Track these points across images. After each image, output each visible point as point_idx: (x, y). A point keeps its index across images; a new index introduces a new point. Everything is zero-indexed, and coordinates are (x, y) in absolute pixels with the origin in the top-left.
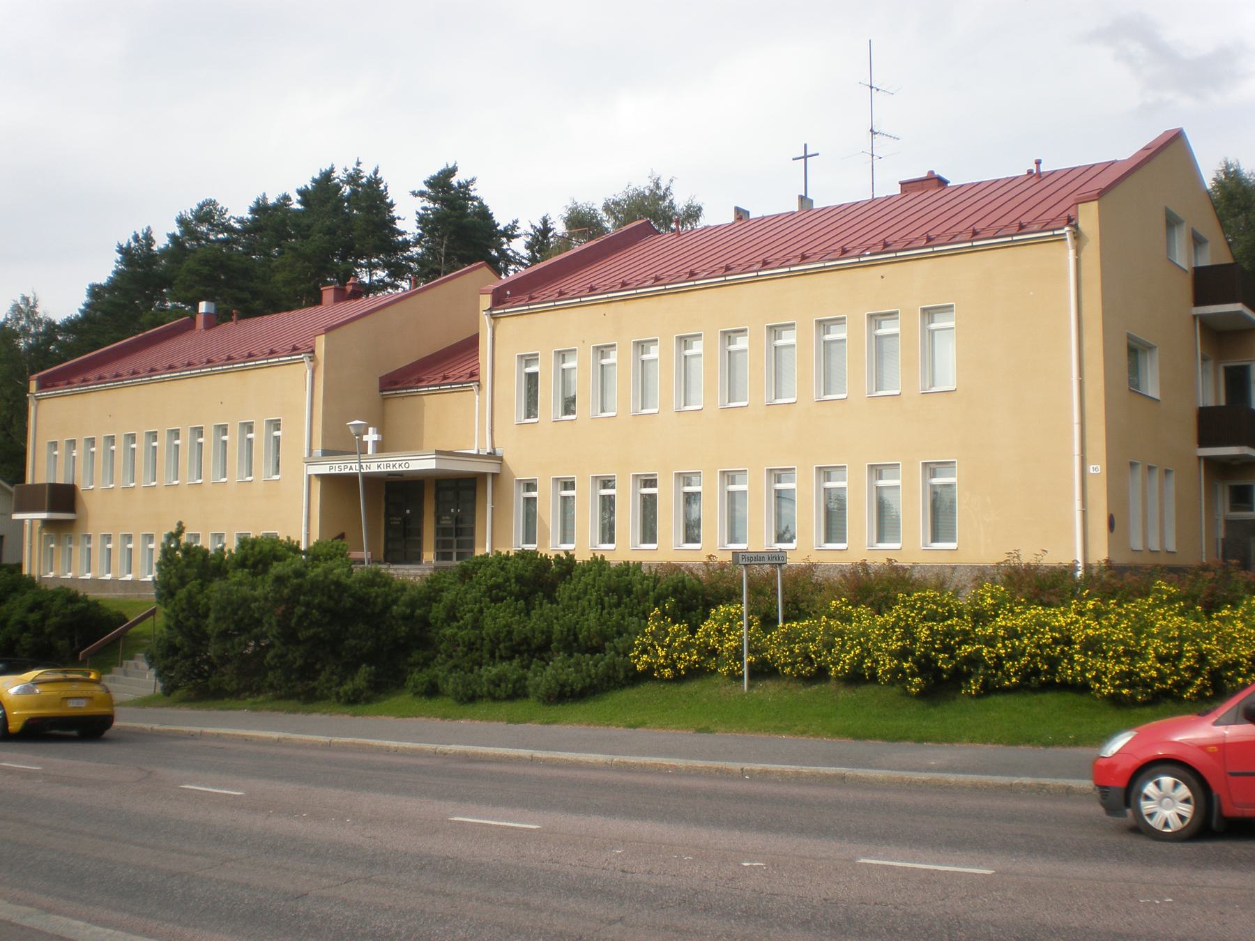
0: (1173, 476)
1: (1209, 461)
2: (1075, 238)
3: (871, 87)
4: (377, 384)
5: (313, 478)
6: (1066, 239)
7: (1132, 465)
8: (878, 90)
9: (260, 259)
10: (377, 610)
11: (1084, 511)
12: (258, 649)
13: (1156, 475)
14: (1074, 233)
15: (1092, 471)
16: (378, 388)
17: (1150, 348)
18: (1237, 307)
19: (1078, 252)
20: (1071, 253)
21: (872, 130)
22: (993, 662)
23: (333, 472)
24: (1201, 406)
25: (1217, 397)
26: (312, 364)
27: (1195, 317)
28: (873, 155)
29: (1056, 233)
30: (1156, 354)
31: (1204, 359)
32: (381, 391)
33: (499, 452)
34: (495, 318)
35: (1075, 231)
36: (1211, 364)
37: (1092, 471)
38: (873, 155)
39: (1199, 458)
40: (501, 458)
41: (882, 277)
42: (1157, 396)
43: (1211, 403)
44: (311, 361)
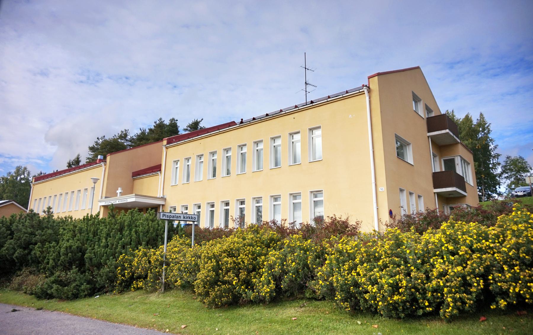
0: (422, 198)
1: (439, 195)
2: (368, 92)
3: (306, 68)
4: (131, 174)
5: (101, 207)
6: (364, 93)
7: (401, 190)
8: (308, 69)
9: (510, 292)
10: (494, 282)
11: (377, 208)
12: (197, 272)
13: (414, 197)
14: (368, 90)
15: (380, 190)
16: (132, 176)
17: (409, 144)
18: (447, 131)
19: (370, 98)
20: (367, 98)
21: (306, 83)
22: (29, 259)
23: (106, 204)
24: (434, 172)
25: (441, 168)
26: (105, 166)
27: (428, 137)
28: (306, 91)
29: (360, 91)
30: (411, 146)
31: (434, 156)
32: (132, 177)
33: (165, 197)
34: (167, 148)
35: (368, 89)
36: (437, 159)
37: (380, 190)
38: (306, 91)
39: (435, 193)
40: (165, 199)
41: (294, 118)
42: (412, 163)
43: (438, 170)
44: (105, 165)
